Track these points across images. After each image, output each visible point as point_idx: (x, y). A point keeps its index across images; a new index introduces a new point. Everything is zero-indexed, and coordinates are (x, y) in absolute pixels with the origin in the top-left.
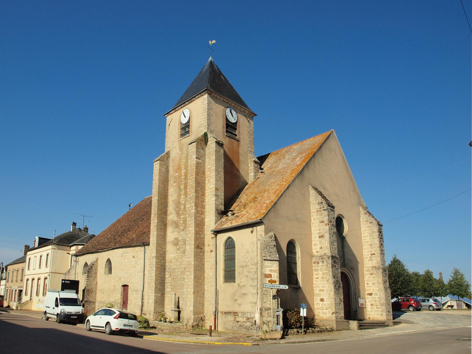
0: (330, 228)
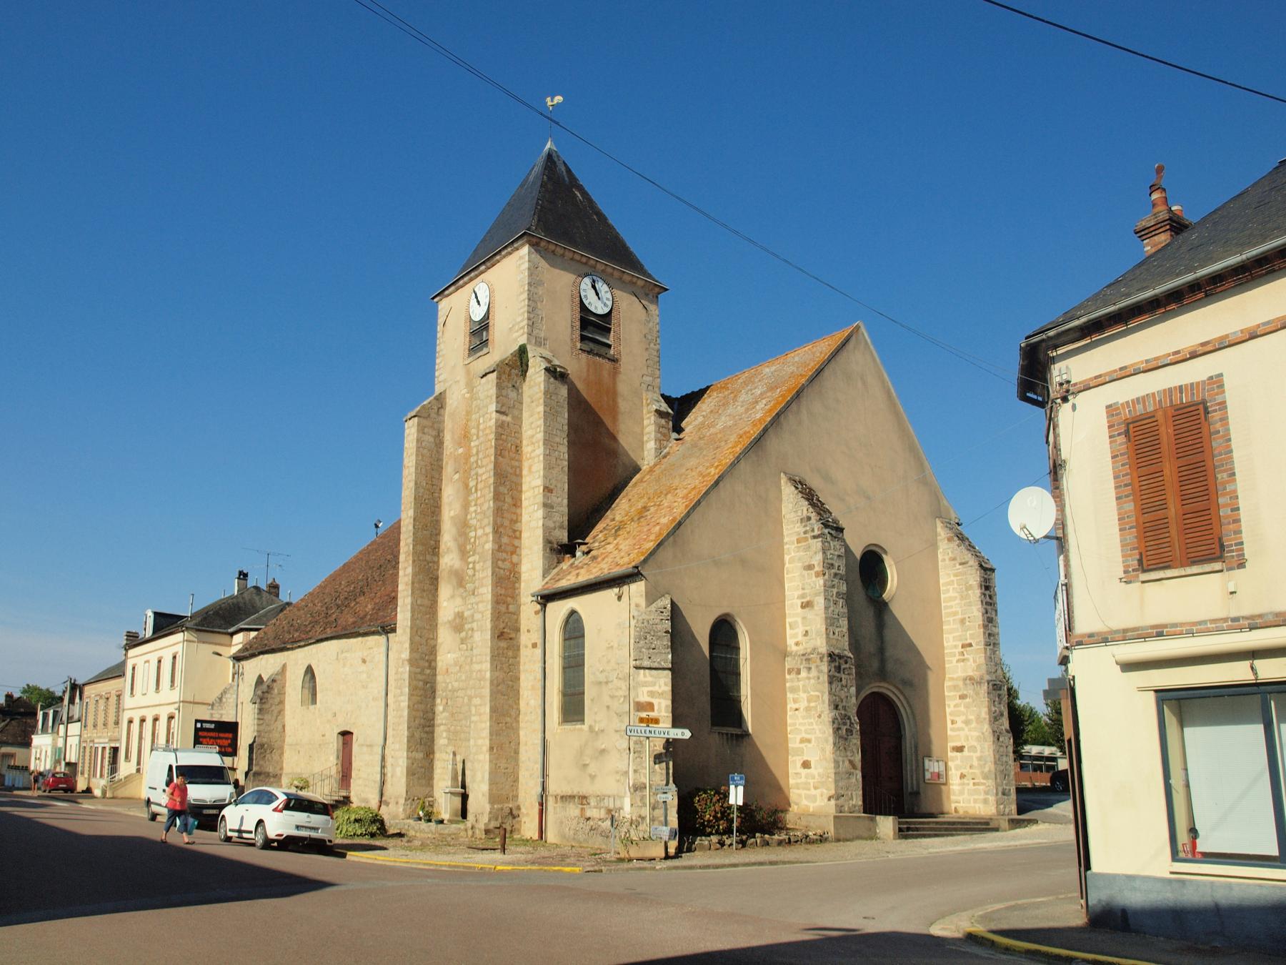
0: (829, 583)
